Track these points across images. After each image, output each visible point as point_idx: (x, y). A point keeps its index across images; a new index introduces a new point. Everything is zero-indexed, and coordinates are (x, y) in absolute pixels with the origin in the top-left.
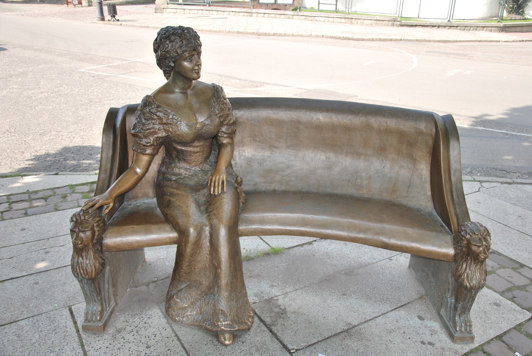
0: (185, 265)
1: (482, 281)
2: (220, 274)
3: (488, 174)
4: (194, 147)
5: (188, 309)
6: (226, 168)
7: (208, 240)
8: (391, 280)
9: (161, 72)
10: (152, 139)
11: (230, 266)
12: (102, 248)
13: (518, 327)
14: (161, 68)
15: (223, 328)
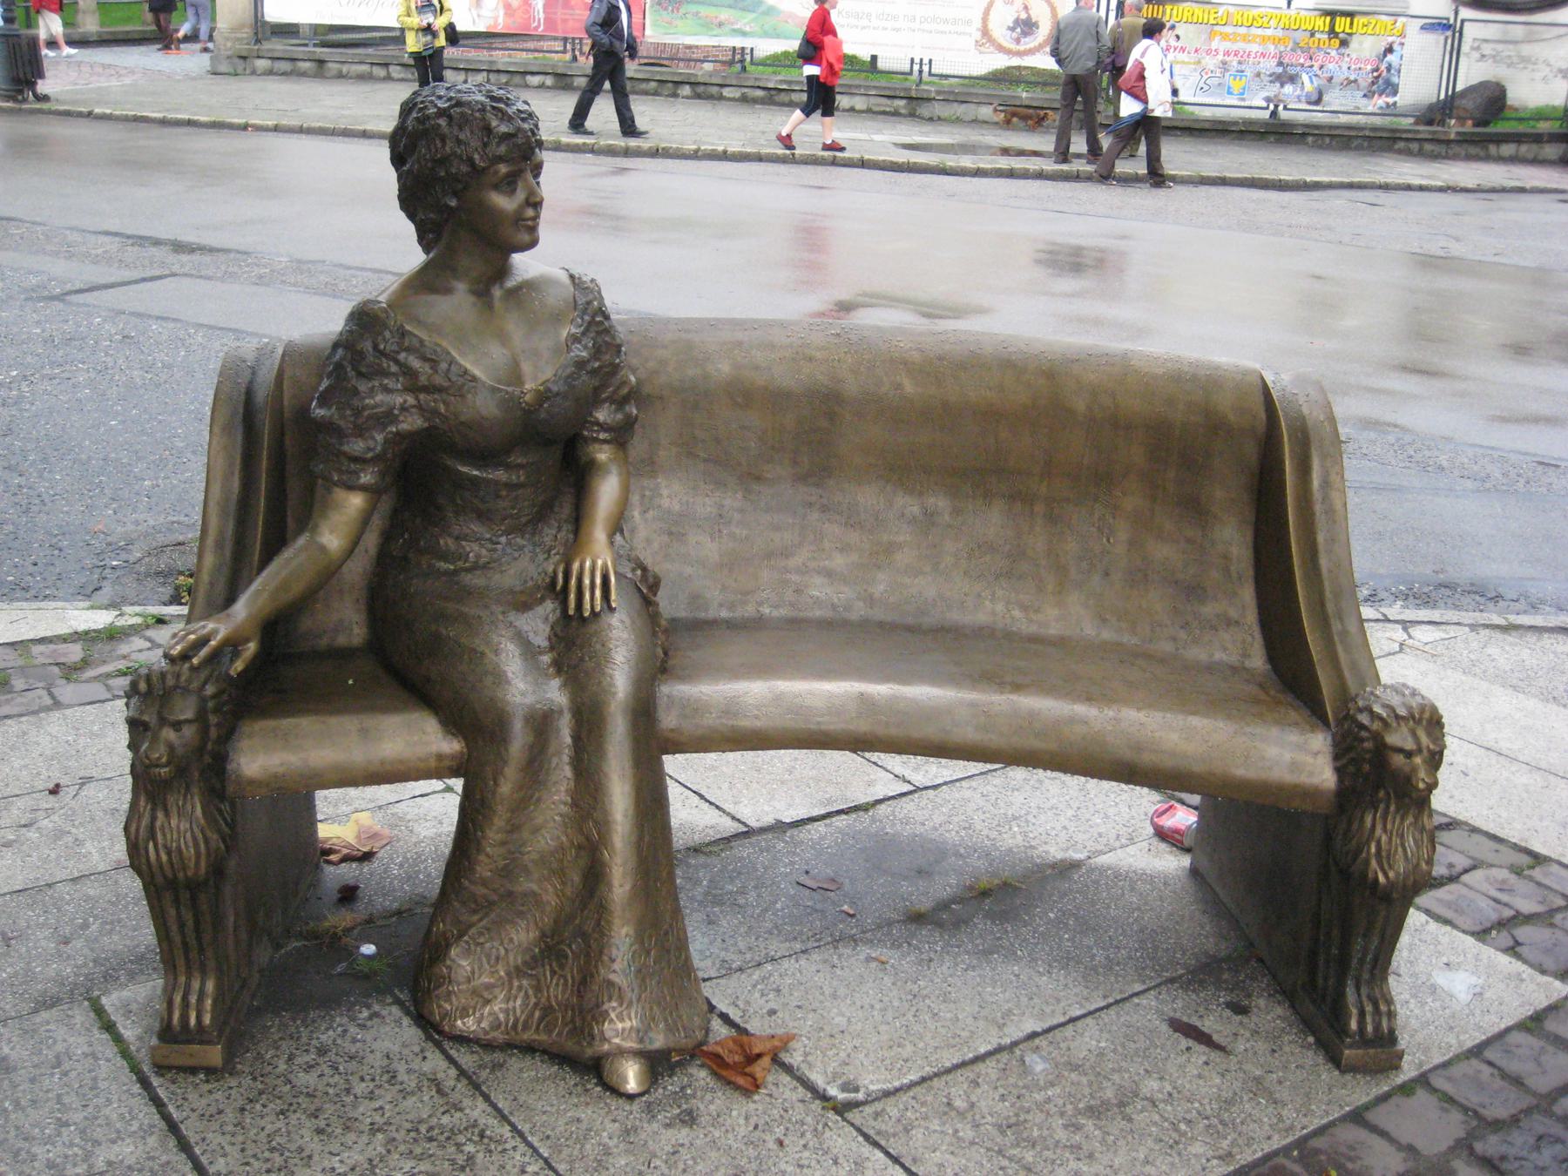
0: (493, 834)
1: (1424, 866)
2: (603, 865)
3: (1426, 601)
4: (508, 467)
5: (497, 991)
6: (611, 536)
7: (566, 759)
8: (1139, 909)
9: (409, 228)
10: (380, 437)
11: (640, 838)
12: (224, 787)
13: (1534, 1023)
14: (411, 216)
15: (617, 1041)
